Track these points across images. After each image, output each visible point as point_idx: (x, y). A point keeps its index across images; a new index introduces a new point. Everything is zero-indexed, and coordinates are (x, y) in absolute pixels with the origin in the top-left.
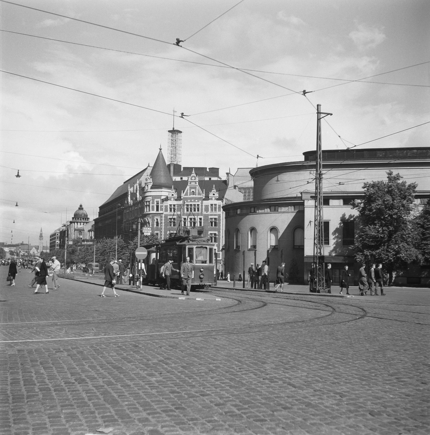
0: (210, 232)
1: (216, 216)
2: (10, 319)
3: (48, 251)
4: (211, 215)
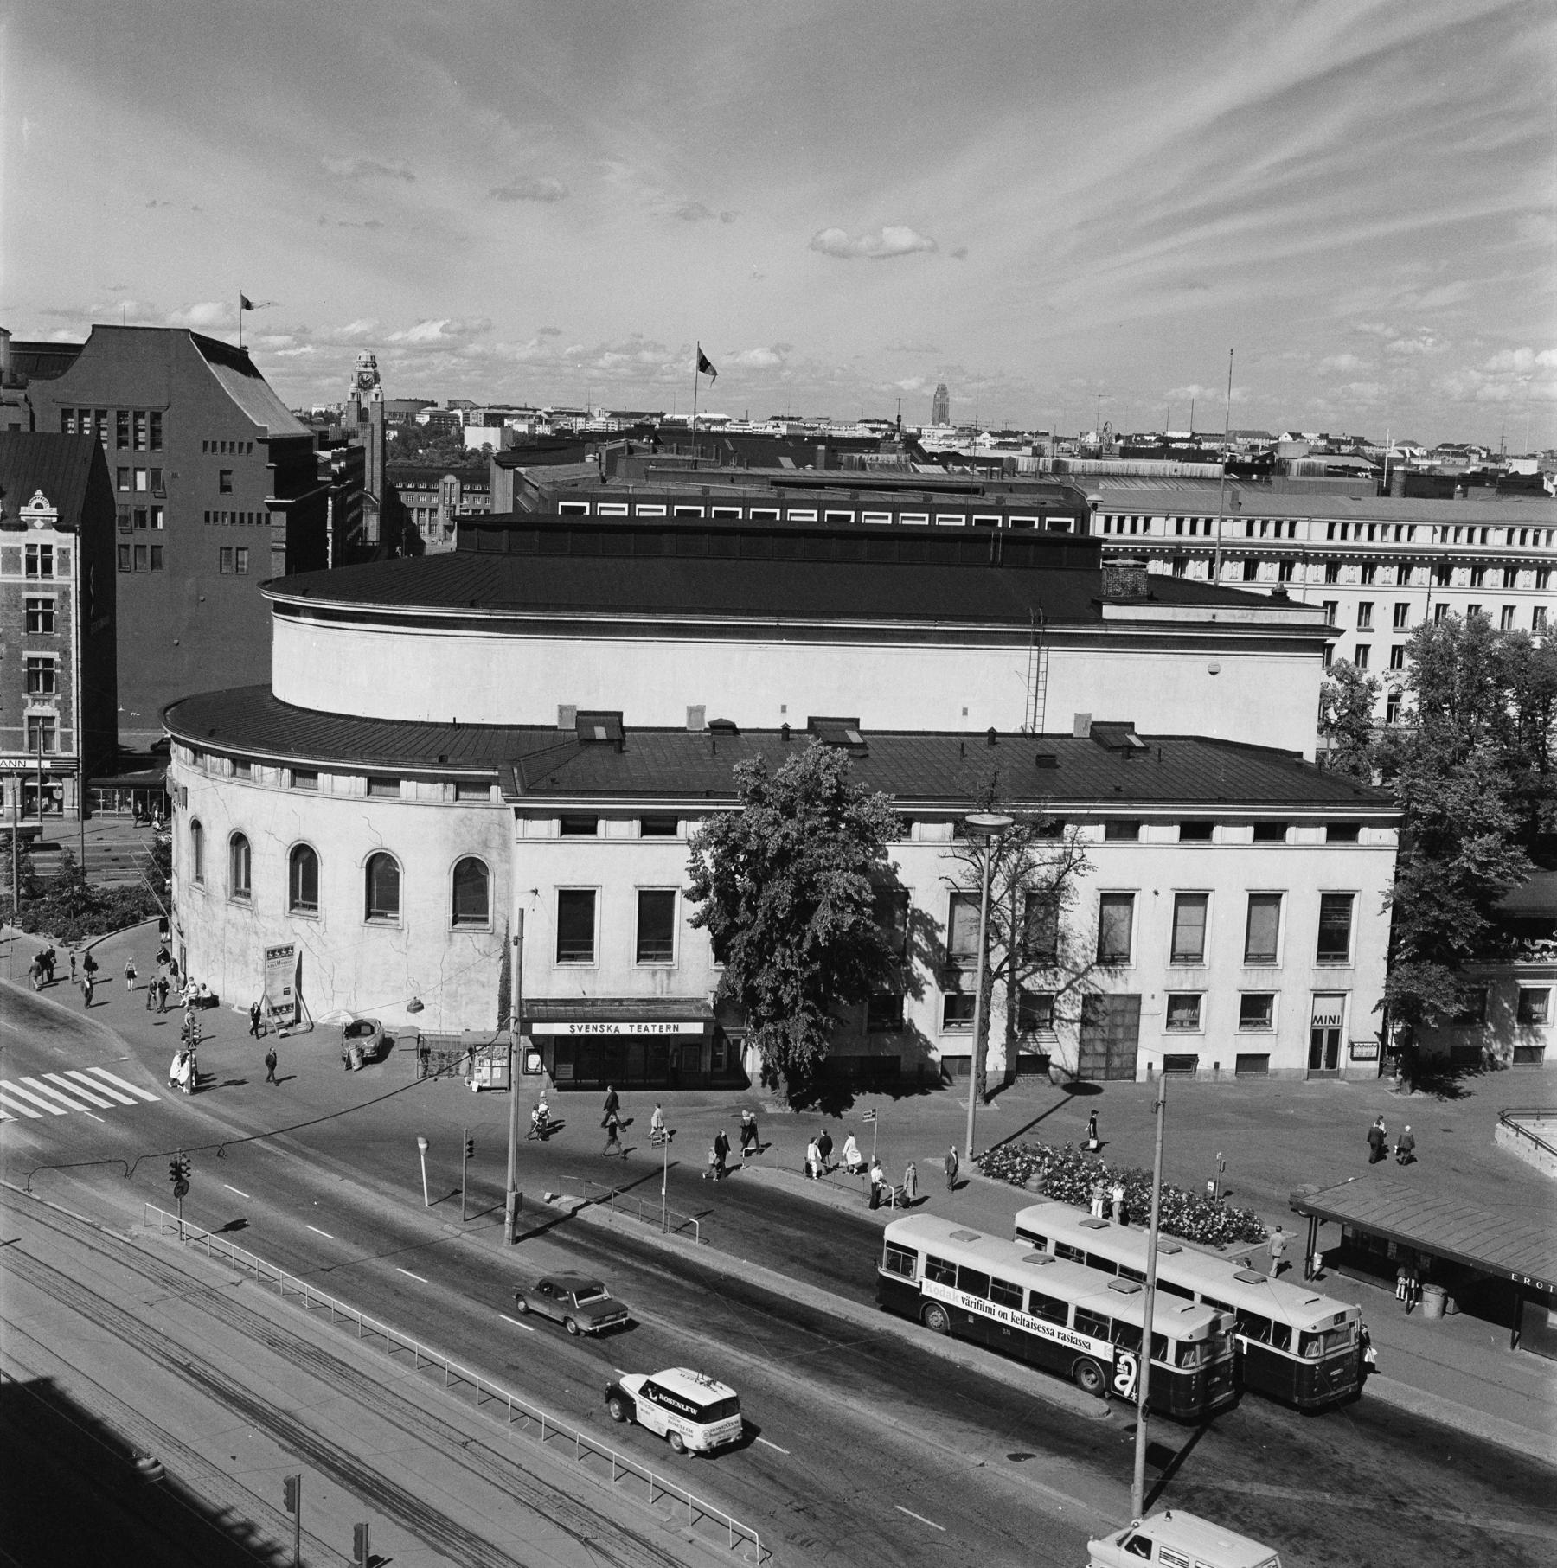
0: (27, 654)
1: (52, 591)
2: (715, 881)
3: (1542, 831)
4: (31, 588)
